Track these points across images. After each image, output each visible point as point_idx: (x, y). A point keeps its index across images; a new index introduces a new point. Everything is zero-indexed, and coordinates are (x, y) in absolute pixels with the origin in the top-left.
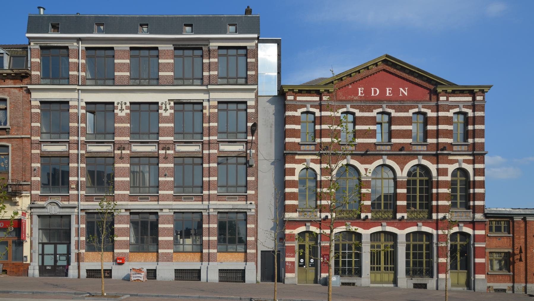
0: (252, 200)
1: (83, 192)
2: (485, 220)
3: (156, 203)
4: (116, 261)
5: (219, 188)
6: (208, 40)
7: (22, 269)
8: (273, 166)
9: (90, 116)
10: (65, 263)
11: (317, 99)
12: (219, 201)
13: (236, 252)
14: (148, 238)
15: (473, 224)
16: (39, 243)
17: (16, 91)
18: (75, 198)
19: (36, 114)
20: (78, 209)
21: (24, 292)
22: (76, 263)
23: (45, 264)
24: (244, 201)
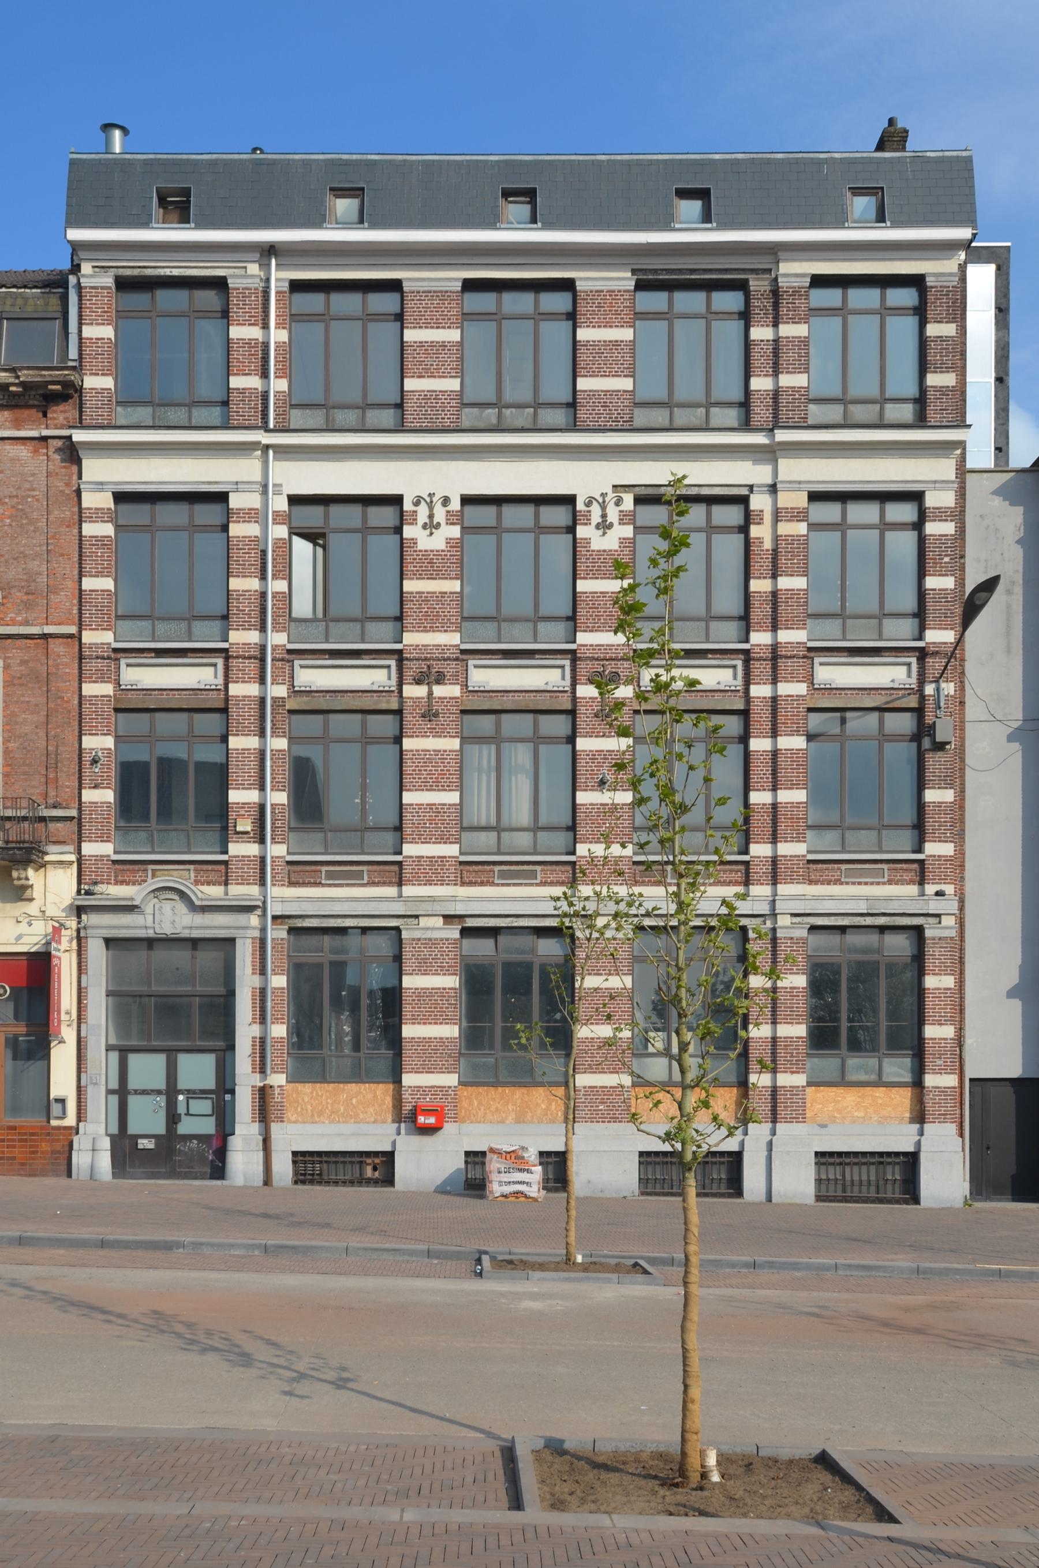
0: (942, 880)
1: (277, 850)
3: (391, 891)
4: (413, 1117)
5: (809, 834)
6: (774, 250)
7: (45, 1147)
8: (1016, 746)
9: (302, 548)
10: (208, 1126)
12: (811, 882)
13: (879, 1083)
14: (531, 1033)
16: (109, 1048)
17: (23, 452)
18: (253, 871)
19: (100, 541)
20: (264, 915)
21: (231, 1246)
22: (255, 1128)
23: (132, 1130)
24: (911, 882)
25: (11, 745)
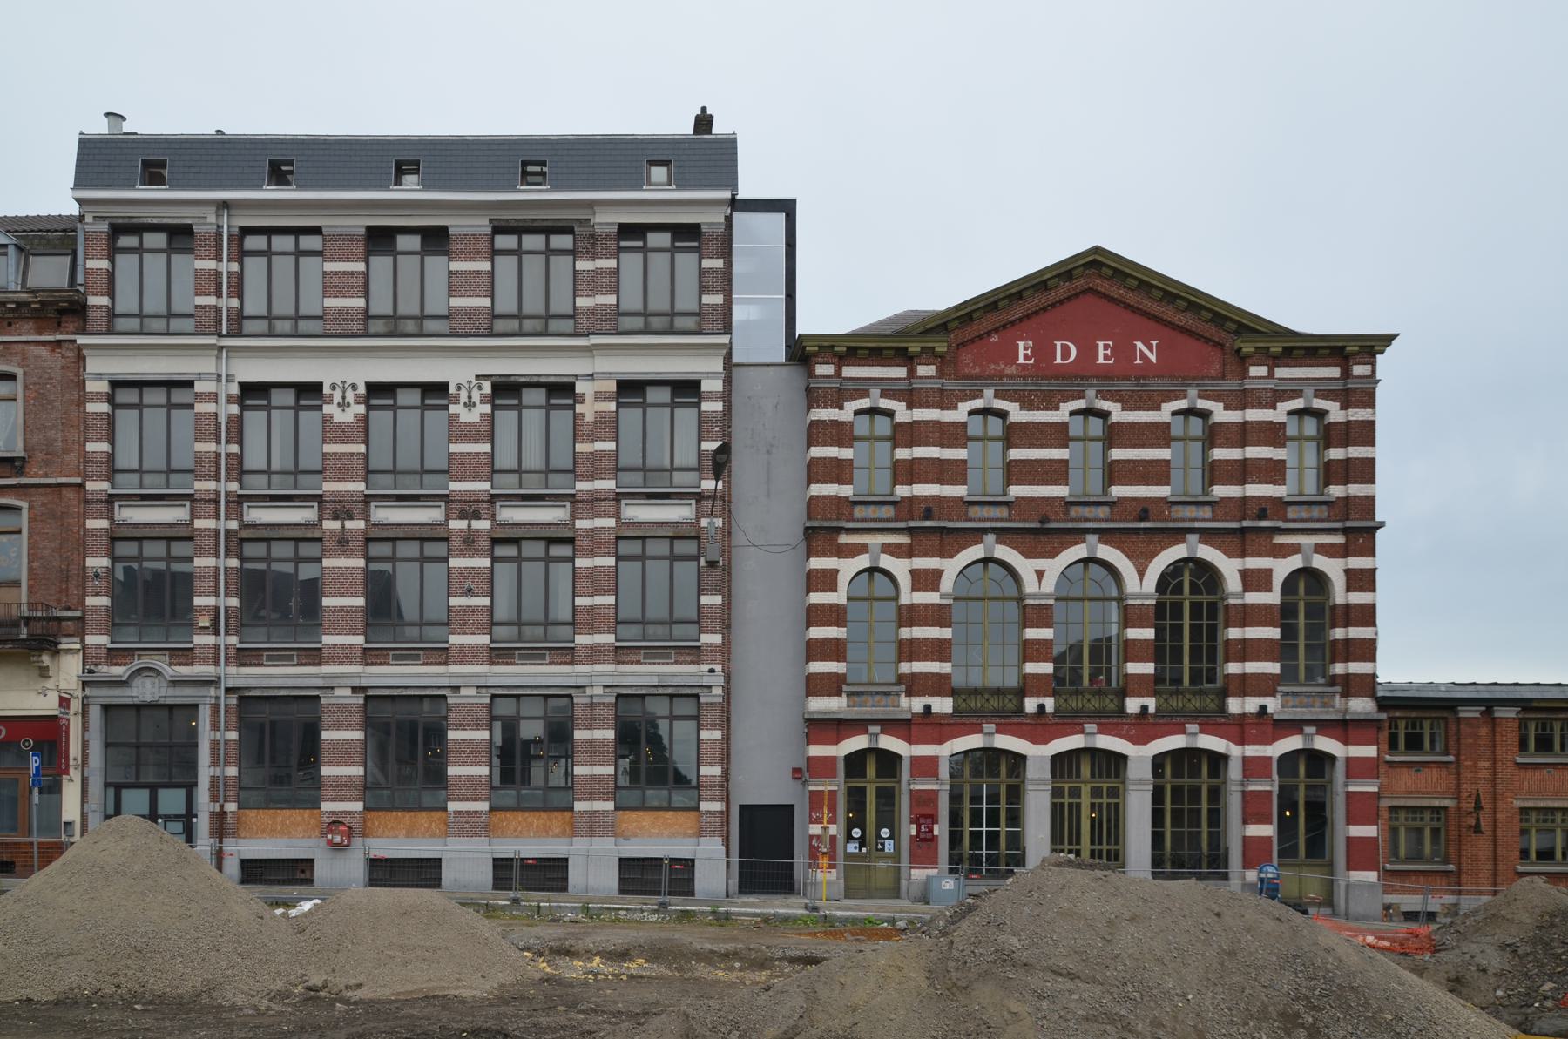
0: (713, 661)
2: (1376, 716)
6: (1213, 520)
11: (1334, 372)
13: (669, 809)
15: (1345, 728)
16: (107, 785)
17: (44, 351)
25: (35, 565)
